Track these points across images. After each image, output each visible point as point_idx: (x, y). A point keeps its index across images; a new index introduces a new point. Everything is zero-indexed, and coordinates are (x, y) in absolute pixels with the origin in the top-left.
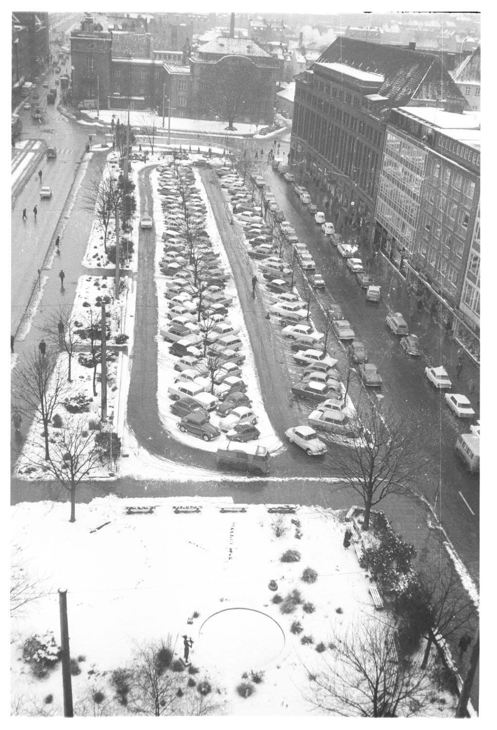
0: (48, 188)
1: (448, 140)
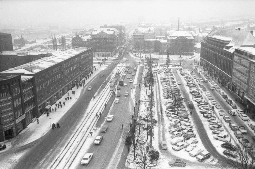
0: (127, 93)
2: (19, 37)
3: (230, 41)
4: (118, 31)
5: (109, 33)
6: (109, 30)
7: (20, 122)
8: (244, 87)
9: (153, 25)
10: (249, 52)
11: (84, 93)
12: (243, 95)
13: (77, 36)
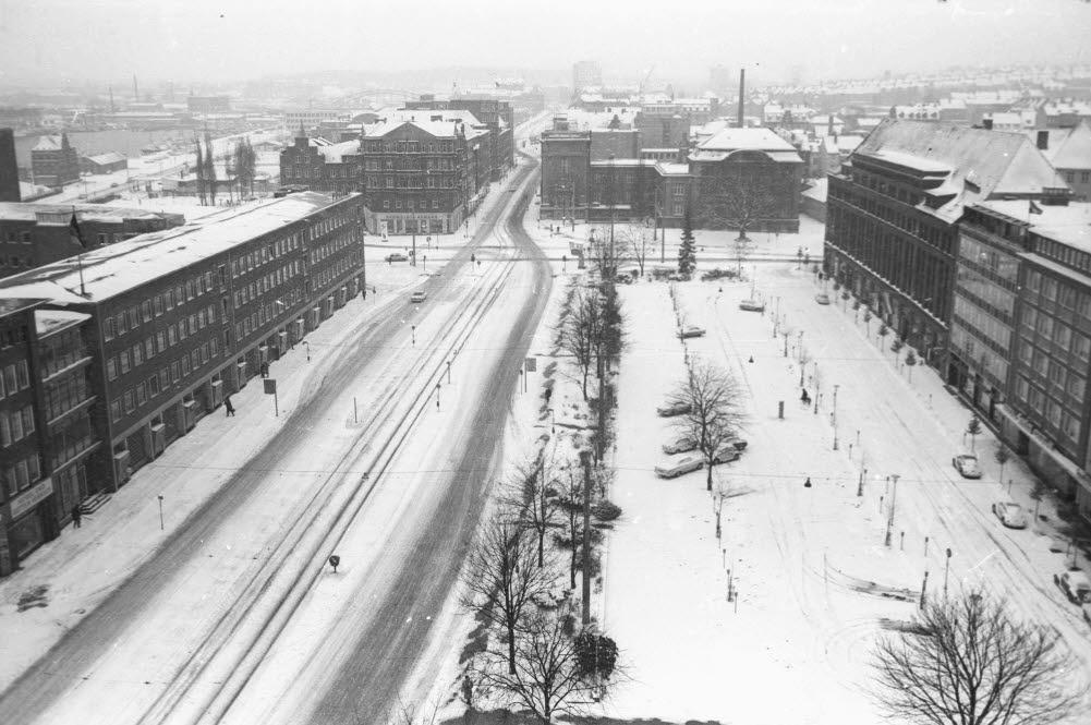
1: (1061, 247)
2: (53, 142)
3: (946, 173)
4: (479, 124)
5: (437, 133)
6: (440, 118)
7: (29, 512)
8: (998, 367)
9: (634, 99)
10: (1018, 221)
11: (368, 339)
12: (993, 402)
13: (302, 141)
